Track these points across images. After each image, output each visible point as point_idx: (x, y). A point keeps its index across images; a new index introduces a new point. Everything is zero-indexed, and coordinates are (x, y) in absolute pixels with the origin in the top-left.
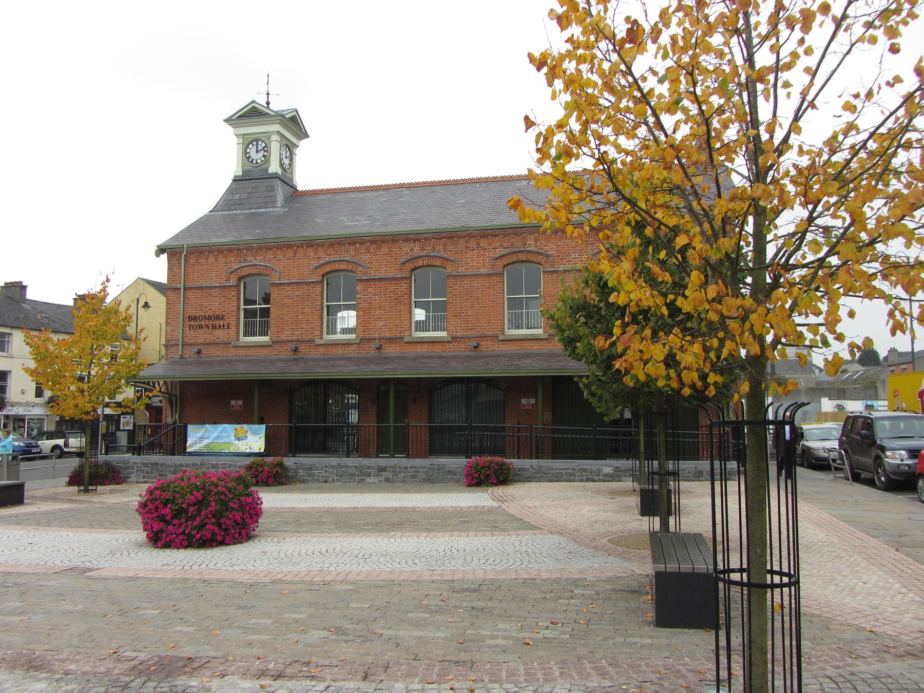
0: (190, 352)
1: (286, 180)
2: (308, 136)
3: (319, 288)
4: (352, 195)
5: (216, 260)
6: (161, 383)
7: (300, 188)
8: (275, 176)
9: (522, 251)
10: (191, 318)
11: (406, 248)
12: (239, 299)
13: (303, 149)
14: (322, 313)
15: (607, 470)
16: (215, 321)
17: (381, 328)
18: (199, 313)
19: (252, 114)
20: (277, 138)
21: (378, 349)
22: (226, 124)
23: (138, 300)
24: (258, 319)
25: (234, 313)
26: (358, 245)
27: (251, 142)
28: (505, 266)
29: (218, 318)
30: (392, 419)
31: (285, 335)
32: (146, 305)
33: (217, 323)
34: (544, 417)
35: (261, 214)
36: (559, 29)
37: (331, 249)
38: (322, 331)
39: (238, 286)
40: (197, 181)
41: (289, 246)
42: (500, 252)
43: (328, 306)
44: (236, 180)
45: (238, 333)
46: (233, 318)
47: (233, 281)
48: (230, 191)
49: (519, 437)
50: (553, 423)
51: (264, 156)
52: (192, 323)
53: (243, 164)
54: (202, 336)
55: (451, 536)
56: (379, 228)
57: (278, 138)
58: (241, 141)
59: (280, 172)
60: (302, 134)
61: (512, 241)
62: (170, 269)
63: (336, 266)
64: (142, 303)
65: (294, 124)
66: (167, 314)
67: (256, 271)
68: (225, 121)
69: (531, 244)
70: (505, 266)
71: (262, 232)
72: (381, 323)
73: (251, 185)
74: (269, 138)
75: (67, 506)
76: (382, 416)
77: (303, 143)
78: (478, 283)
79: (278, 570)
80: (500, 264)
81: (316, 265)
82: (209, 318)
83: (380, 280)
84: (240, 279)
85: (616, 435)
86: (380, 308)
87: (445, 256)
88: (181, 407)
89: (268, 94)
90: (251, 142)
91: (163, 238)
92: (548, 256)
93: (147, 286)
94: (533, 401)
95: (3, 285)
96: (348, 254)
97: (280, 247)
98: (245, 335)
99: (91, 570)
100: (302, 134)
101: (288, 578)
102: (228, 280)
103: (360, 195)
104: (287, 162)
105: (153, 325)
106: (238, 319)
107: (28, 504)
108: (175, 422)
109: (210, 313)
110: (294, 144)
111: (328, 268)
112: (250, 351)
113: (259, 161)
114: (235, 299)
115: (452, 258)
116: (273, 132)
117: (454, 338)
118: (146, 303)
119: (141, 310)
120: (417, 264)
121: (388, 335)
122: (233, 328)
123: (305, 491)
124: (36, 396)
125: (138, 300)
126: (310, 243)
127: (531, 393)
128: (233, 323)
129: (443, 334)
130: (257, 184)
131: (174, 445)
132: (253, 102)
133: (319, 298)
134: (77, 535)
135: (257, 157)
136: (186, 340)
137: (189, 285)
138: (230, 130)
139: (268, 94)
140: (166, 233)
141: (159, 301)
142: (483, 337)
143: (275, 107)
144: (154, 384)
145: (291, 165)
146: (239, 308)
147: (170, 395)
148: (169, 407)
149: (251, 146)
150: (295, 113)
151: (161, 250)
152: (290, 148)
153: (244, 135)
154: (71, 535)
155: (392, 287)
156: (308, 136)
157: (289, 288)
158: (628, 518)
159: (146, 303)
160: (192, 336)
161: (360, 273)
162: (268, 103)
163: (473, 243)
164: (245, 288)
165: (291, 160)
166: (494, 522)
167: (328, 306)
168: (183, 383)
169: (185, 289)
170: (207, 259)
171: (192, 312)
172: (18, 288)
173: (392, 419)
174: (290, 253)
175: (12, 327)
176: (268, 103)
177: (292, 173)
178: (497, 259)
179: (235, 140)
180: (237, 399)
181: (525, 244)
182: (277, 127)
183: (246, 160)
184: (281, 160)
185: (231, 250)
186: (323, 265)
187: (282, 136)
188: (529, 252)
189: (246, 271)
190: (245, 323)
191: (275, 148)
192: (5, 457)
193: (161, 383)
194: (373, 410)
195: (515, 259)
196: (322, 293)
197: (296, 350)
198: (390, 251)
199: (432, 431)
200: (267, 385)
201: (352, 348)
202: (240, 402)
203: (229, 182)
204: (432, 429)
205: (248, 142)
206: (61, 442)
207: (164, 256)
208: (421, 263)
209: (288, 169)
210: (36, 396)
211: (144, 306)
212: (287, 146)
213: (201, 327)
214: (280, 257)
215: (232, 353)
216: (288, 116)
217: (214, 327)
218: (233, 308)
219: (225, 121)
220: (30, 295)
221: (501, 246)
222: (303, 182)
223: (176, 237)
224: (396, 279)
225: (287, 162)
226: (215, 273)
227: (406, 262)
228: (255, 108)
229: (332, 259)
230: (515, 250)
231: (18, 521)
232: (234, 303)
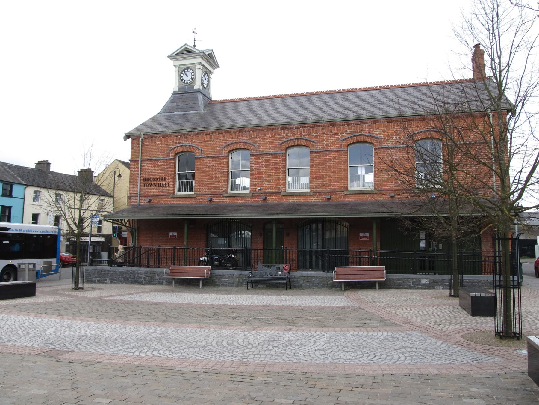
0: (144, 202)
1: (205, 92)
2: (219, 67)
4: (247, 102)
5: (161, 142)
6: (126, 220)
7: (213, 99)
8: (199, 91)
9: (360, 135)
10: (145, 180)
11: (283, 134)
12: (175, 167)
13: (216, 74)
14: (228, 176)
15: (424, 281)
16: (160, 181)
17: (267, 185)
18: (150, 177)
21: (264, 199)
22: (168, 59)
23: (115, 172)
24: (185, 183)
25: (172, 177)
26: (251, 132)
28: (348, 145)
29: (162, 179)
30: (274, 246)
31: (204, 190)
32: (120, 176)
33: (161, 182)
34: (376, 245)
35: (189, 115)
37: (234, 135)
38: (228, 188)
39: (175, 159)
40: (150, 97)
41: (207, 133)
42: (345, 136)
43: (231, 172)
45: (174, 189)
46: (171, 180)
47: (171, 156)
48: (172, 101)
50: (381, 250)
51: (192, 79)
52: (146, 183)
53: (179, 84)
54: (152, 191)
56: (264, 121)
57: (201, 67)
58: (178, 69)
59: (201, 88)
60: (215, 66)
61: (353, 128)
62: (132, 148)
63: (238, 146)
64: (117, 174)
65: (210, 58)
66: (130, 177)
67: (186, 149)
68: (168, 57)
69: (366, 129)
70: (348, 145)
71: (190, 126)
72: (266, 183)
73: (184, 97)
74: (195, 67)
75: (61, 299)
76: (267, 242)
77: (216, 71)
78: (330, 156)
79: (208, 359)
80: (345, 143)
81: (224, 145)
82: (156, 179)
83: (266, 155)
85: (424, 257)
86: (266, 173)
87: (308, 139)
88: (138, 236)
89: (195, 40)
91: (129, 128)
92: (378, 138)
93: (121, 164)
94: (367, 235)
95: (37, 162)
97: (202, 134)
98: (179, 191)
99: (66, 352)
100: (215, 66)
101: (218, 368)
102: (168, 155)
103: (251, 102)
104: (206, 82)
105: (123, 190)
106: (175, 180)
107: (38, 296)
108: (134, 246)
109: (157, 176)
110: (210, 71)
111: (232, 147)
112: (181, 199)
113: (189, 82)
114: (172, 167)
115: (313, 140)
116: (198, 63)
117: (315, 193)
118: (120, 174)
119: (117, 179)
120: (290, 145)
121: (270, 190)
122: (171, 186)
123: (218, 292)
124: (10, 208)
125: (115, 172)
126: (220, 131)
127: (369, 229)
128: (171, 183)
130: (186, 97)
131: (134, 260)
132: (186, 45)
133: (226, 166)
134: (62, 321)
135: (187, 78)
136: (142, 193)
137: (144, 158)
138: (171, 63)
139: (195, 40)
140: (131, 126)
141: (126, 172)
142: (333, 192)
144: (122, 221)
145: (208, 85)
146: (175, 173)
147: (132, 228)
148: (131, 236)
150: (211, 52)
151: (127, 137)
152: (207, 73)
153: (179, 65)
154: (58, 321)
155: (273, 160)
156: (219, 67)
157: (207, 160)
158: (393, 311)
159: (120, 174)
160: (145, 190)
162: (195, 46)
163: (327, 130)
164: (179, 160)
165: (208, 82)
166: (366, 321)
167: (231, 172)
168: (139, 220)
169: (141, 161)
170: (155, 141)
171: (146, 176)
172: (46, 165)
173: (274, 246)
174: (207, 138)
175: (41, 187)
176: (195, 46)
177: (209, 90)
178: (343, 140)
179: (174, 69)
180: (173, 231)
181: (362, 130)
182: (200, 60)
183: (181, 81)
184: (202, 81)
185: (171, 136)
186: (229, 145)
187: (203, 66)
188: (365, 135)
189: (180, 150)
190: (179, 183)
191: (199, 73)
192: (27, 265)
193: (126, 220)
194: (260, 240)
195: (355, 140)
196: (228, 163)
197: (211, 200)
198: (272, 135)
199: (300, 253)
200: (193, 222)
201: (248, 199)
202: (175, 234)
204: (299, 252)
205: (183, 70)
207: (129, 141)
208: (292, 143)
209: (206, 87)
210: (10, 208)
211: (118, 176)
212: (206, 72)
213: (151, 185)
214: (202, 140)
215: (171, 202)
216: (207, 53)
217: (159, 185)
218: (170, 171)
220: (52, 169)
221: (346, 132)
222: (216, 95)
223: (137, 128)
224: (276, 154)
226: (161, 150)
227: (283, 143)
228: (186, 48)
229: (235, 141)
230: (355, 134)
231: (27, 310)
232: (172, 170)
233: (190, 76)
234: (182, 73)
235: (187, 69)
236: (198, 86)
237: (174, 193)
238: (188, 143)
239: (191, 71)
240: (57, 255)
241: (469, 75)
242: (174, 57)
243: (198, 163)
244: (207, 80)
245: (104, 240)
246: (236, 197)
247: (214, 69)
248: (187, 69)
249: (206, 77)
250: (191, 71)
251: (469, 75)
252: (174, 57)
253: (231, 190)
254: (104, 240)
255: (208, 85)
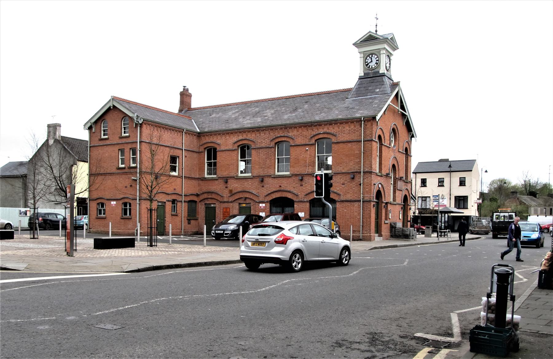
3: (273, 150)
19: (370, 39)
27: (369, 56)
43: (318, 156)
44: (360, 78)
49: (26, 206)
51: (376, 63)
53: (364, 69)
57: (384, 52)
58: (362, 55)
60: (395, 48)
63: (283, 139)
65: (391, 42)
68: (354, 44)
74: (379, 52)
84: (316, 141)
90: (369, 56)
96: (332, 129)
100: (395, 48)
110: (391, 54)
113: (373, 67)
129: (250, 174)
132: (370, 32)
135: (373, 65)
138: (356, 50)
145: (389, 67)
149: (368, 58)
161: (334, 140)
162: (376, 31)
165: (390, 64)
176: (376, 31)
180: (301, 212)
203: (356, 79)
205: (367, 56)
206: (409, 223)
219: (354, 44)
225: (388, 65)
228: (370, 35)
233: (374, 61)
235: (372, 54)
236: (382, 70)
238: (251, 136)
239: (376, 57)
241: (193, 107)
243: (218, 154)
248: (372, 54)
250: (376, 57)
251: (193, 107)
253: (278, 172)
255: (389, 67)
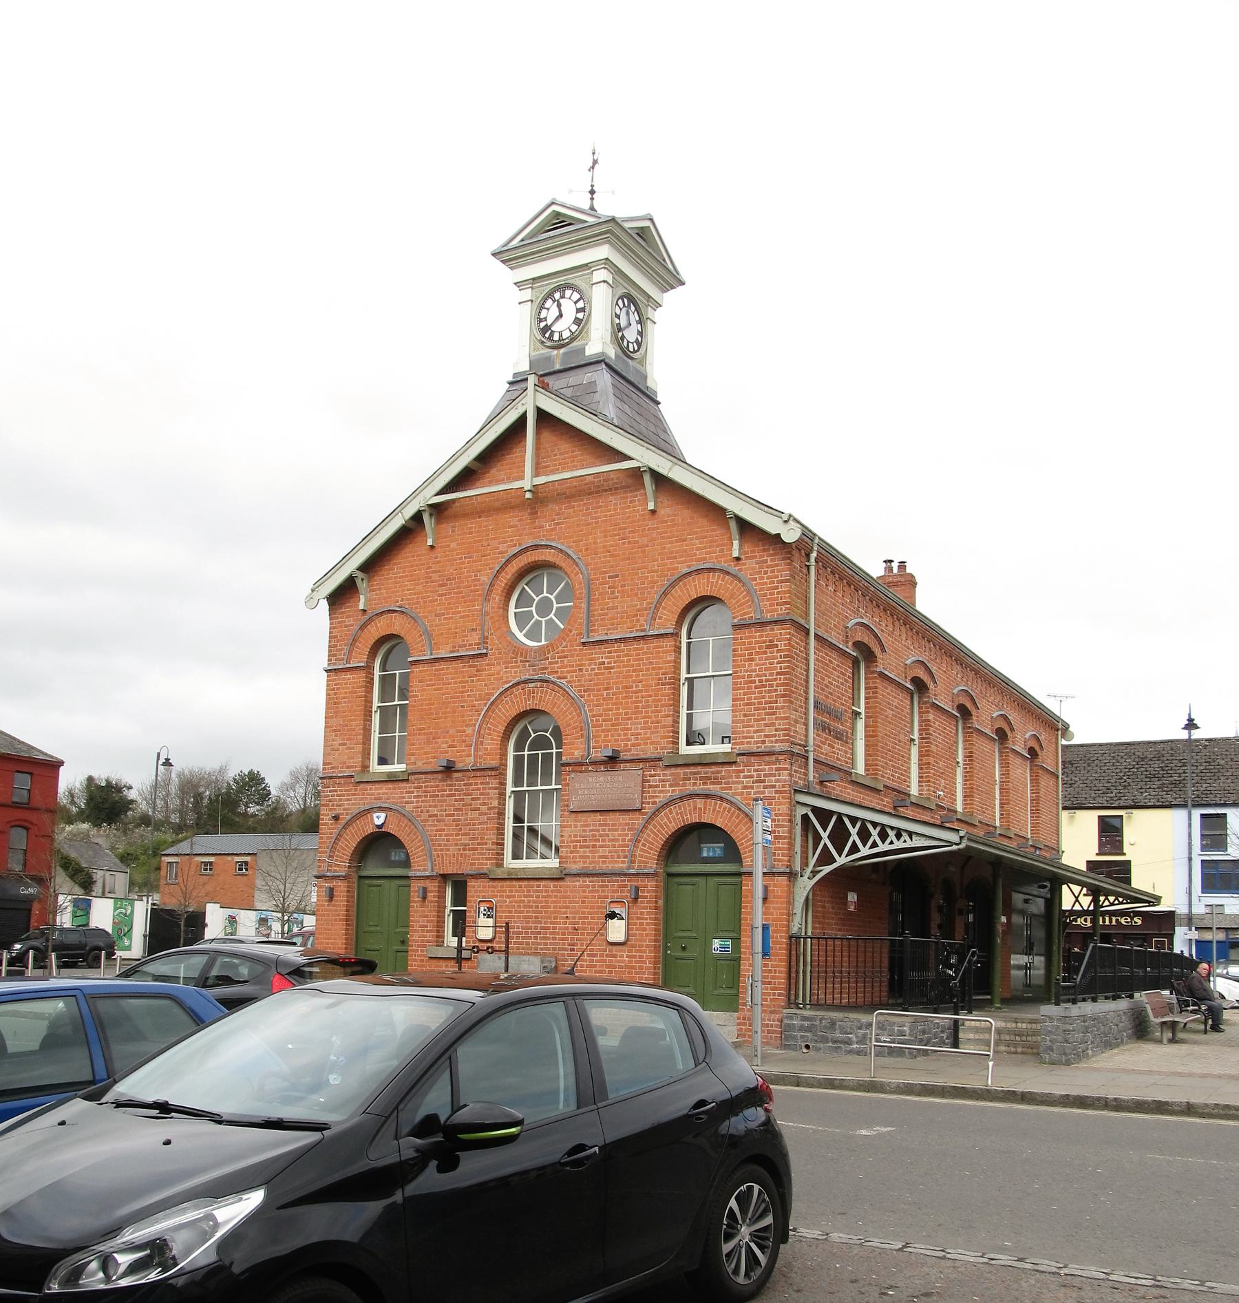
13: (672, 317)
19: (557, 227)
20: (601, 275)
22: (497, 263)
27: (550, 295)
36: (747, 414)
55: (764, 550)
59: (611, 352)
60: (670, 279)
64: (162, 760)
65: (641, 241)
68: (494, 255)
77: (670, 299)
89: (592, 192)
90: (550, 295)
100: (670, 279)
104: (631, 335)
118: (167, 760)
138: (506, 276)
139: (592, 192)
143: (606, 208)
152: (633, 301)
159: (167, 760)
177: (642, 361)
187: (619, 272)
191: (602, 300)
211: (164, 764)
228: (557, 214)
234: (542, 307)
237: (365, 767)
239: (576, 296)
240: (997, 982)
242: (508, 256)
244: (635, 327)
245: (1177, 950)
246: (498, 510)
247: (665, 290)
249: (634, 317)
250: (576, 296)
252: (508, 256)
254: (1177, 950)
